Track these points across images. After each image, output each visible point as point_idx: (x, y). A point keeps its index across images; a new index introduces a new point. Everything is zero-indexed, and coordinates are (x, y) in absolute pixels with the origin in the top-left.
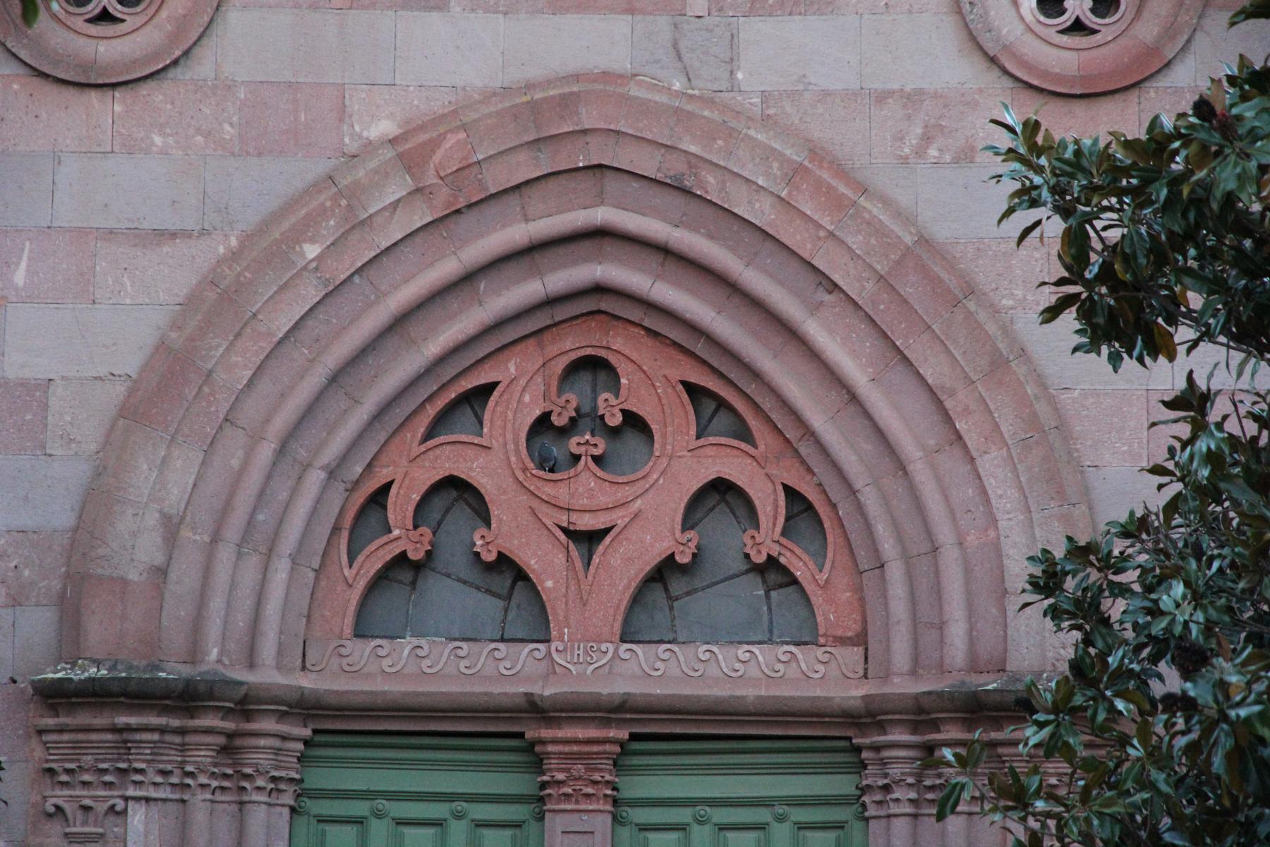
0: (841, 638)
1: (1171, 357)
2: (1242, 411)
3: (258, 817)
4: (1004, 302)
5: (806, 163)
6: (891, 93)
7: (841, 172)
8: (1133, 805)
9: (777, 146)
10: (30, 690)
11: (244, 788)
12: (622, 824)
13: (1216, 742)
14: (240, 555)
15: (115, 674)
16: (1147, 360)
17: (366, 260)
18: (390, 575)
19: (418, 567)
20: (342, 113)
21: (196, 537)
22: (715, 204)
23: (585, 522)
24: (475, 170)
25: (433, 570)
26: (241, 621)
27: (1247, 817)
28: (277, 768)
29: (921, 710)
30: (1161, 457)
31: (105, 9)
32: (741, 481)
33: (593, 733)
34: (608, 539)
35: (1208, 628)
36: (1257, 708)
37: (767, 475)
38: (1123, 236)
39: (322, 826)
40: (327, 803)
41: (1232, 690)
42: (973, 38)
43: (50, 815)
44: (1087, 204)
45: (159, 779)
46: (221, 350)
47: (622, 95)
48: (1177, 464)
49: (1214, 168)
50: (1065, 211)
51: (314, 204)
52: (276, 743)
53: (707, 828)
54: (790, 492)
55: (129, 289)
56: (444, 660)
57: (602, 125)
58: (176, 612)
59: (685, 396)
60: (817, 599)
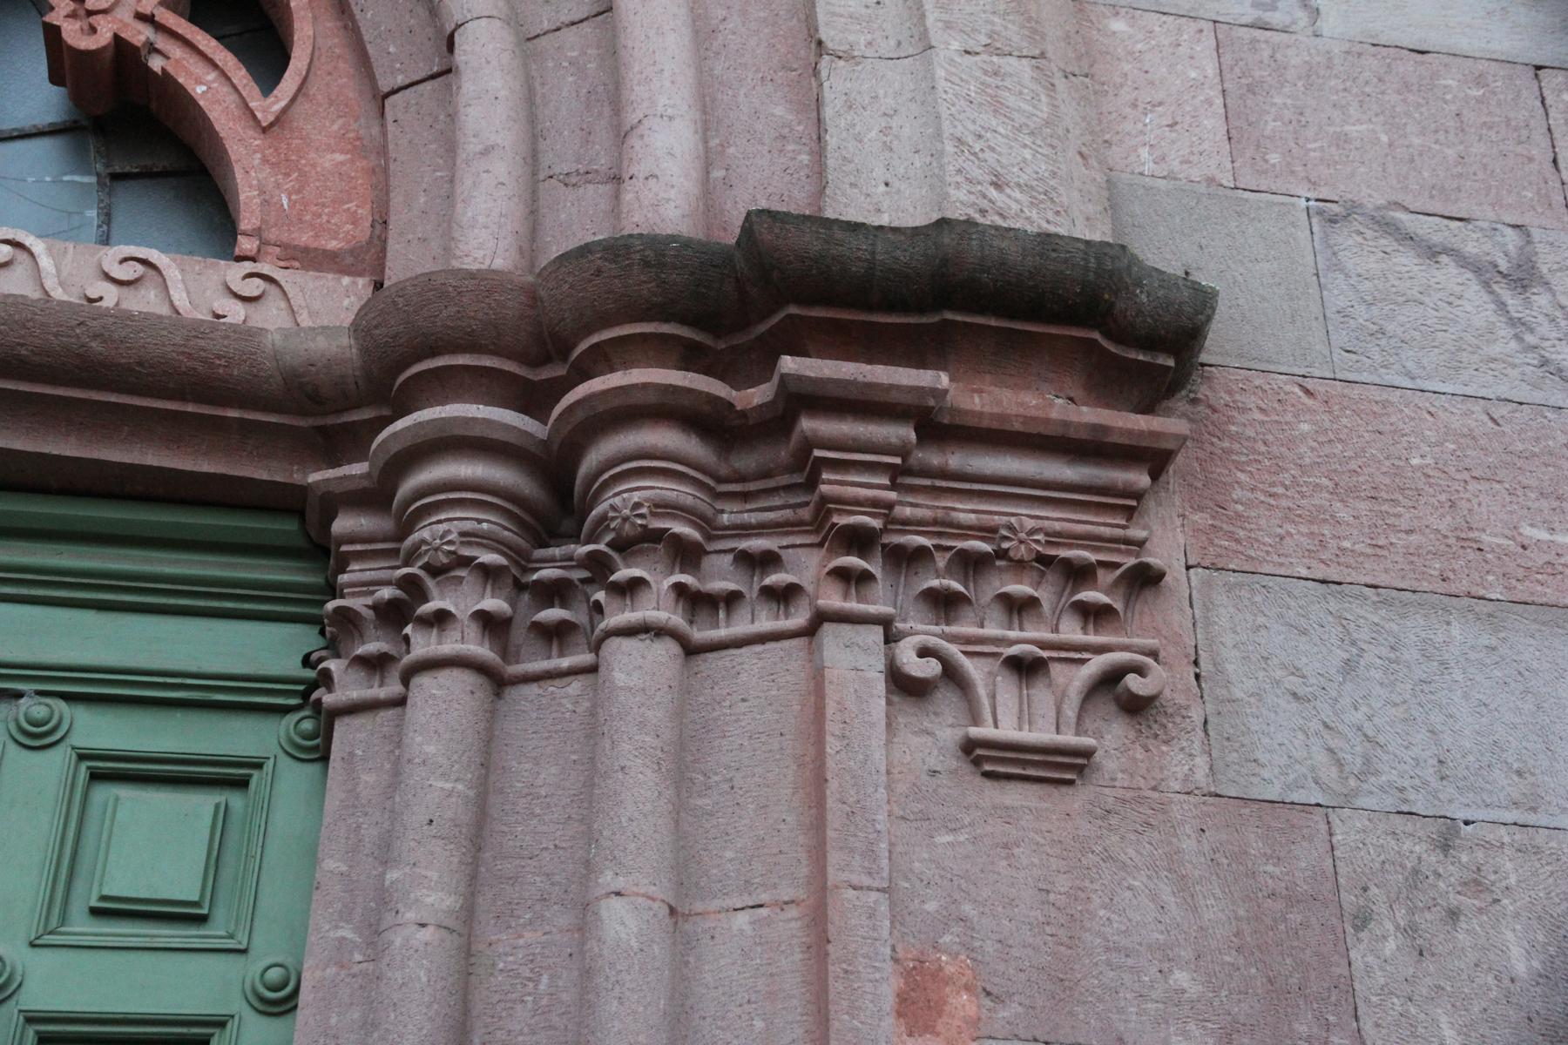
0: (306, 250)
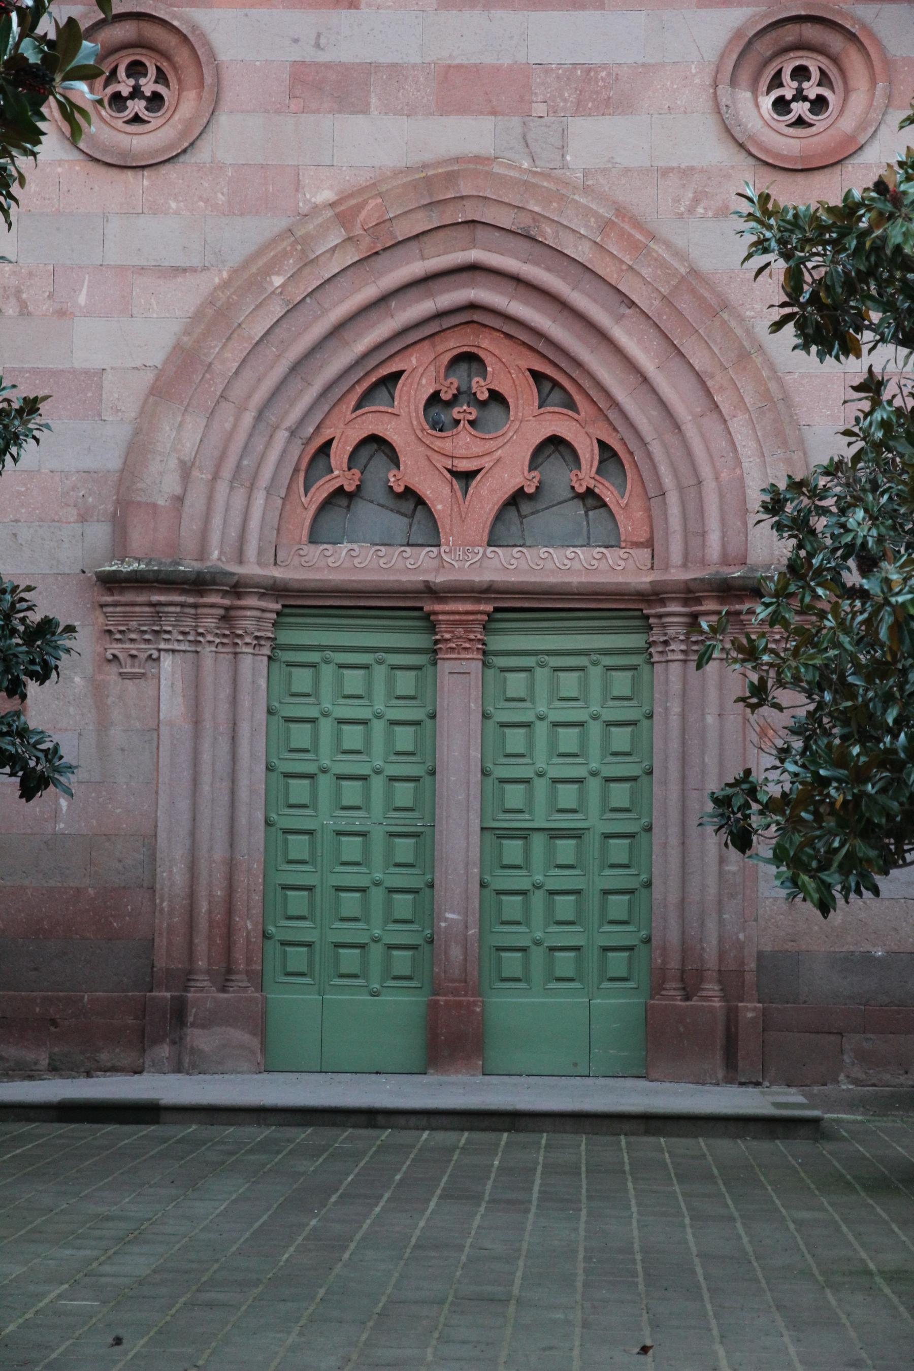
1: (858, 355)
2: (905, 393)
3: (246, 662)
4: (748, 313)
5: (613, 218)
6: (672, 169)
7: (637, 224)
8: (828, 658)
9: (594, 206)
10: (95, 578)
11: (237, 644)
12: (488, 667)
13: (882, 619)
14: (232, 488)
15: (150, 568)
16: (842, 358)
17: (314, 287)
18: (334, 501)
19: (351, 496)
20: (298, 187)
21: (201, 476)
22: (551, 247)
23: (464, 466)
24: (388, 224)
25: (361, 498)
26: (233, 533)
27: (903, 666)
28: (259, 630)
29: (689, 591)
30: (850, 425)
31: (136, 114)
32: (568, 437)
33: (469, 607)
34: (479, 477)
35: (880, 540)
36: (909, 596)
37: (586, 433)
38: (826, 273)
39: (289, 668)
40: (291, 653)
41: (893, 584)
42: (728, 130)
43: (109, 661)
44: (802, 251)
45: (181, 638)
46: (217, 349)
47: (487, 172)
48: (861, 429)
49: (887, 228)
50: (787, 256)
51: (280, 248)
52: (257, 613)
53: (546, 670)
54: (602, 445)
55: (155, 307)
56: (369, 559)
57: (475, 193)
58: (190, 527)
59: (531, 380)
60: (620, 517)
